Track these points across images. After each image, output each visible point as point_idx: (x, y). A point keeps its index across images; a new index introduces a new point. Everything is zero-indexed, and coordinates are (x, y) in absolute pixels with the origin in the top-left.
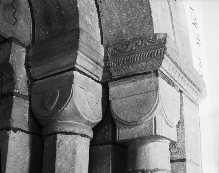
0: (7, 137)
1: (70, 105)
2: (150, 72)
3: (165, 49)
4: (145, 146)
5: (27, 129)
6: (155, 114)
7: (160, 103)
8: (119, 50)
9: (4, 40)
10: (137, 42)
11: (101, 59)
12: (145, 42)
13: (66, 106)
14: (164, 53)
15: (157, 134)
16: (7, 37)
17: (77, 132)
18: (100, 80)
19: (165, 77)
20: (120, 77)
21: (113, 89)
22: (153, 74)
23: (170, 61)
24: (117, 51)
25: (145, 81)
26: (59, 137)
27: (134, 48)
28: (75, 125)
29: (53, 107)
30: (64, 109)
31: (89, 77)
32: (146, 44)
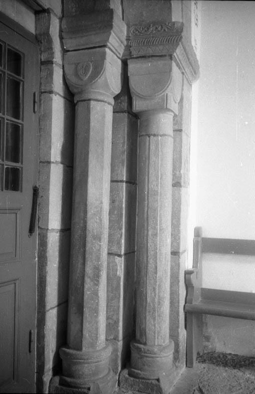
0: (51, 99)
1: (103, 78)
2: (165, 56)
3: (181, 37)
4: (161, 114)
5: (62, 95)
6: (167, 92)
7: (172, 84)
8: (140, 31)
9: (42, 9)
10: (157, 26)
11: (124, 38)
12: (164, 27)
13: (100, 78)
14: (180, 41)
15: (168, 107)
16: (46, 8)
17: (105, 100)
18: (121, 57)
19: (176, 61)
20: (138, 56)
21: (131, 66)
22: (167, 58)
23: (182, 48)
24: (139, 32)
25: (160, 63)
26: (92, 103)
27: (154, 32)
28: (104, 94)
29: (87, 77)
30: (97, 80)
31: (115, 53)
32: (165, 30)
